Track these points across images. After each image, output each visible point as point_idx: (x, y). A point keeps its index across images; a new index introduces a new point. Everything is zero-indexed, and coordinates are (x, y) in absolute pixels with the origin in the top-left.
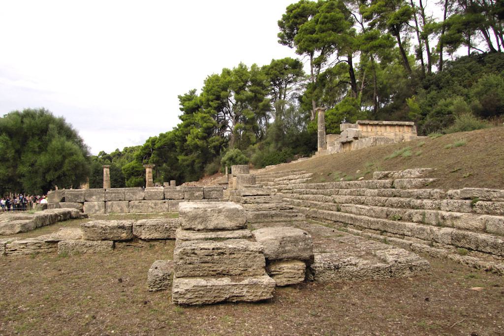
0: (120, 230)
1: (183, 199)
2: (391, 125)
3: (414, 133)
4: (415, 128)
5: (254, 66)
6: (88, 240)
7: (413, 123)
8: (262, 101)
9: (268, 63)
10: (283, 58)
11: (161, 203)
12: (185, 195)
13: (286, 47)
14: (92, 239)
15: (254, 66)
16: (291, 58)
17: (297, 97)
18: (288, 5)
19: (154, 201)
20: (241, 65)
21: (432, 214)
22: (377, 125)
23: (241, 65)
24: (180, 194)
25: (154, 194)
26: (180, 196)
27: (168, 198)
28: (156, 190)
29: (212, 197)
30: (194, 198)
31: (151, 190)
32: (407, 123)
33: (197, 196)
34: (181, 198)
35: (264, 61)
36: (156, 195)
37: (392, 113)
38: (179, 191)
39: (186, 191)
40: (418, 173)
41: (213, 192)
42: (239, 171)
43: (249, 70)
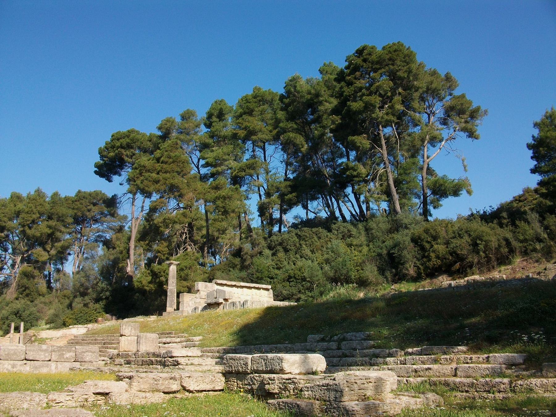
0: (171, 381)
1: (50, 360)
2: (255, 288)
3: (271, 298)
4: (271, 291)
5: (56, 194)
6: (140, 391)
7: (270, 287)
8: (60, 241)
9: (72, 194)
10: (93, 190)
11: (21, 365)
12: (53, 356)
13: (103, 180)
14: (143, 390)
15: (56, 194)
16: (103, 192)
17: (102, 241)
18: (115, 131)
19: (12, 362)
20: (38, 191)
21: (403, 368)
22: (255, 288)
23: (38, 191)
24: (47, 355)
25: (12, 352)
26: (46, 357)
27: (31, 358)
28: (16, 348)
29: (86, 360)
30: (63, 360)
31: (10, 348)
32: (264, 286)
33: (67, 358)
34: (47, 359)
35: (68, 191)
36: (15, 353)
37: (32, 258)
38: (46, 351)
39: (54, 351)
40: (363, 337)
41: (87, 353)
42: (130, 329)
43: (47, 199)
